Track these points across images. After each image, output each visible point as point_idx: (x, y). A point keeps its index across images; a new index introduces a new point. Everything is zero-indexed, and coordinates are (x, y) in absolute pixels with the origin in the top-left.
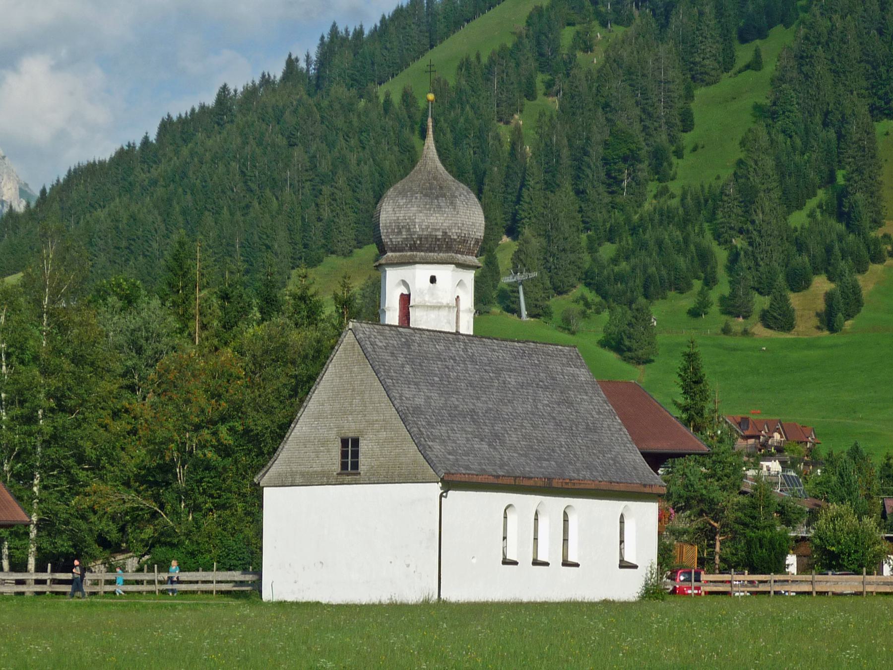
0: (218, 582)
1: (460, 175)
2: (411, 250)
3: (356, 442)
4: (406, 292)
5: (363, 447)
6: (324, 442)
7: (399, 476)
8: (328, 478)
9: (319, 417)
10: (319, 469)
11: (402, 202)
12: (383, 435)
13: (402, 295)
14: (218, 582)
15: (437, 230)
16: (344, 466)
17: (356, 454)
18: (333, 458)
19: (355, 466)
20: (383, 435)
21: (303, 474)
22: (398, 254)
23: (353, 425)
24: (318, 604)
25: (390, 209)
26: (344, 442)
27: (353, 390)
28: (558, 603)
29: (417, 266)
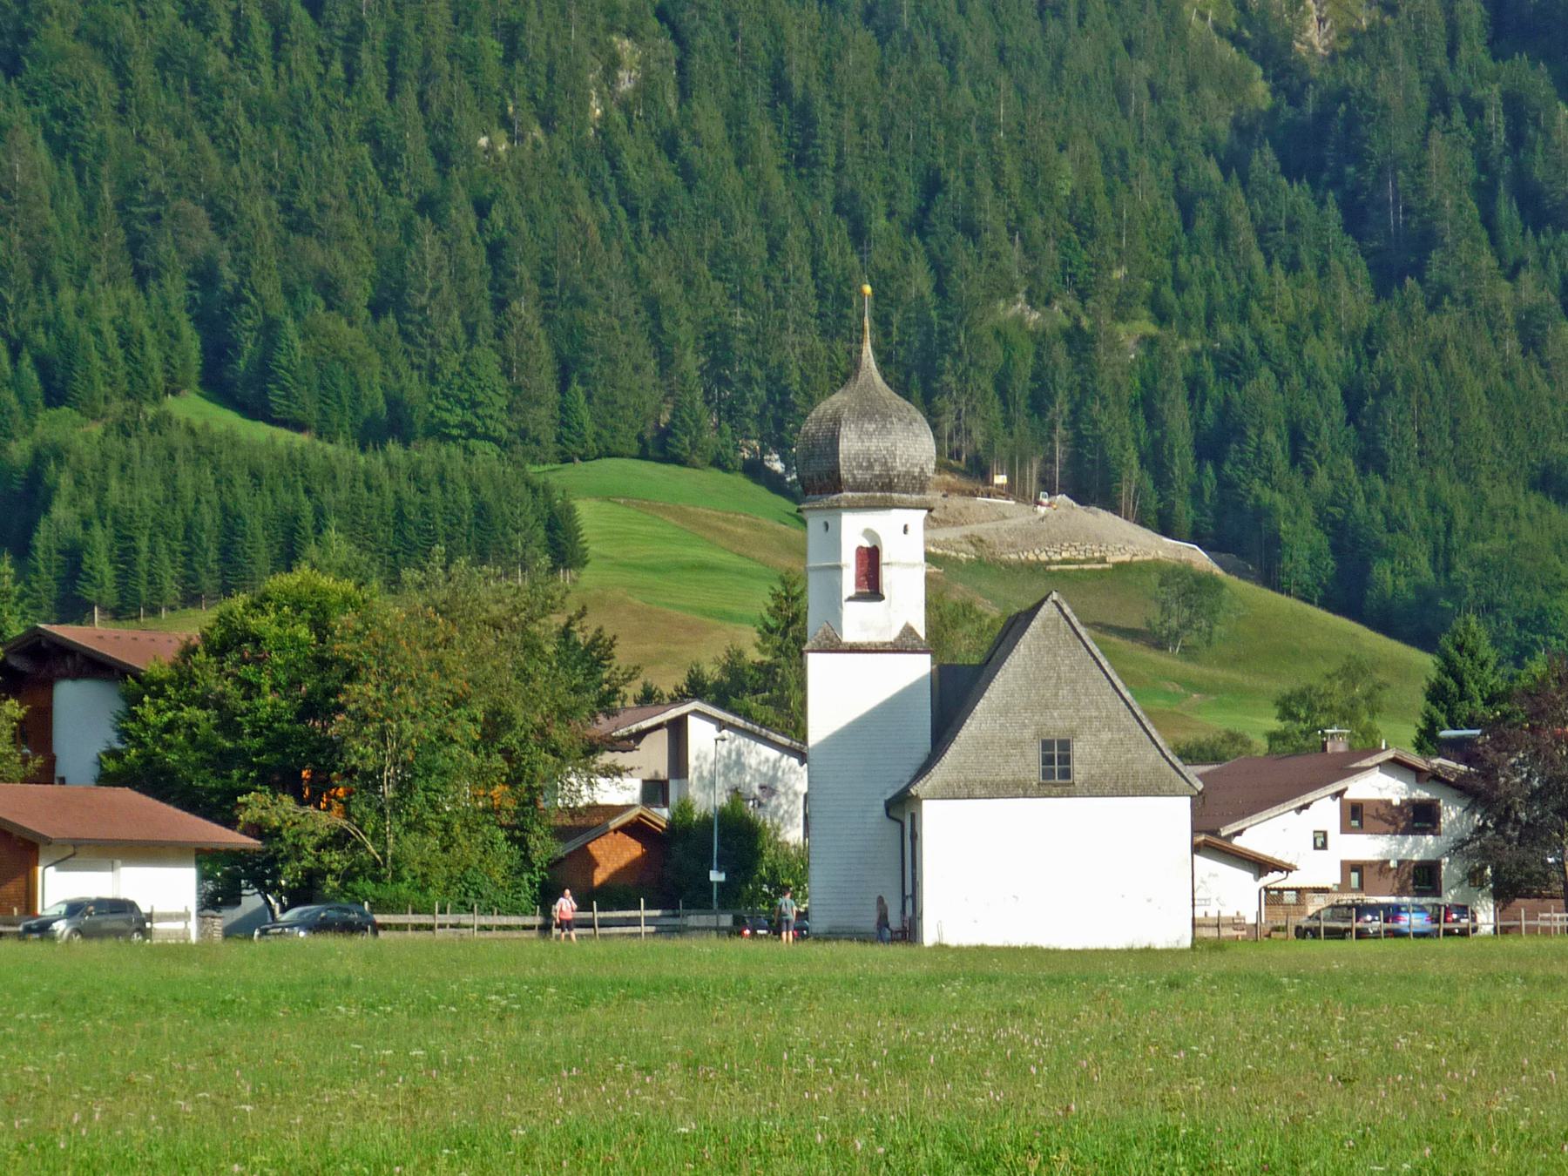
0: (400, 927)
1: (903, 390)
2: (882, 489)
3: (1065, 745)
4: (867, 544)
5: (1078, 750)
6: (1017, 744)
7: (1134, 787)
8: (1025, 790)
9: (1006, 710)
10: (1010, 778)
11: (871, 427)
12: (1106, 736)
13: (860, 550)
14: (400, 927)
15: (913, 465)
16: (1047, 774)
17: (1066, 760)
18: (1030, 764)
19: (1066, 774)
20: (1106, 736)
21: (984, 784)
22: (860, 494)
23: (1060, 724)
24: (1148, 951)
25: (853, 436)
26: (1047, 745)
27: (1059, 678)
28: (1096, 951)
29: (895, 512)
